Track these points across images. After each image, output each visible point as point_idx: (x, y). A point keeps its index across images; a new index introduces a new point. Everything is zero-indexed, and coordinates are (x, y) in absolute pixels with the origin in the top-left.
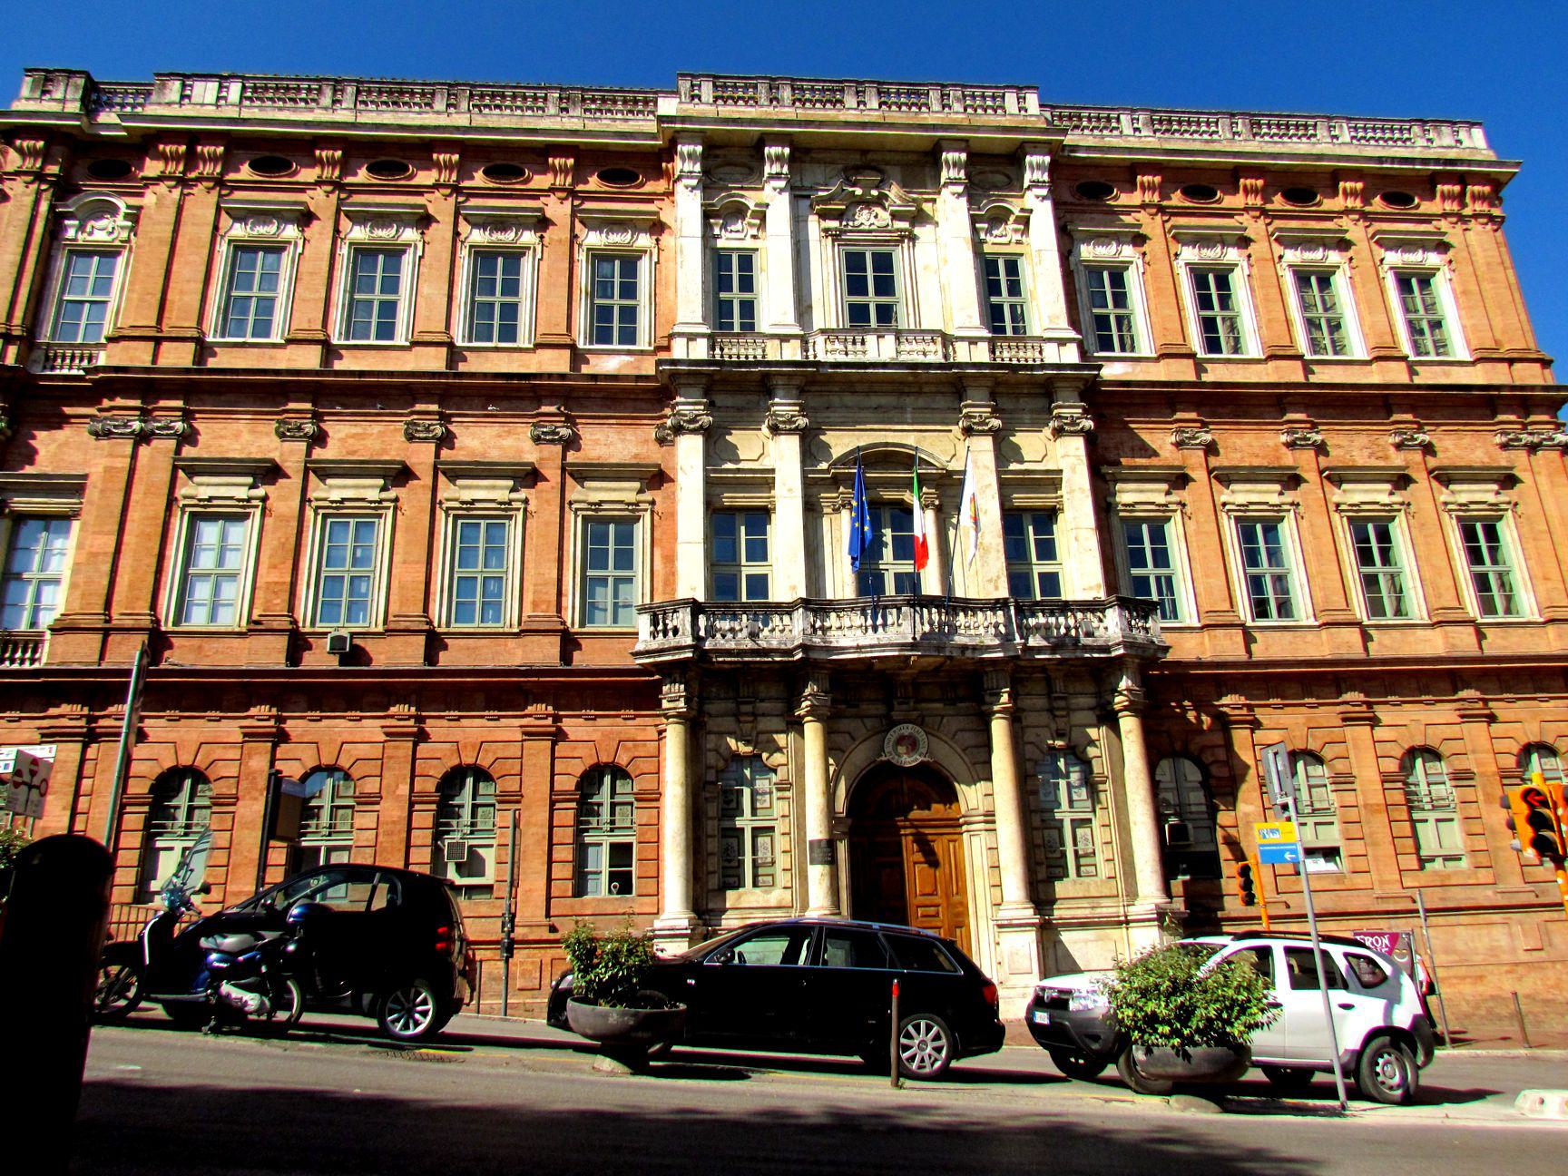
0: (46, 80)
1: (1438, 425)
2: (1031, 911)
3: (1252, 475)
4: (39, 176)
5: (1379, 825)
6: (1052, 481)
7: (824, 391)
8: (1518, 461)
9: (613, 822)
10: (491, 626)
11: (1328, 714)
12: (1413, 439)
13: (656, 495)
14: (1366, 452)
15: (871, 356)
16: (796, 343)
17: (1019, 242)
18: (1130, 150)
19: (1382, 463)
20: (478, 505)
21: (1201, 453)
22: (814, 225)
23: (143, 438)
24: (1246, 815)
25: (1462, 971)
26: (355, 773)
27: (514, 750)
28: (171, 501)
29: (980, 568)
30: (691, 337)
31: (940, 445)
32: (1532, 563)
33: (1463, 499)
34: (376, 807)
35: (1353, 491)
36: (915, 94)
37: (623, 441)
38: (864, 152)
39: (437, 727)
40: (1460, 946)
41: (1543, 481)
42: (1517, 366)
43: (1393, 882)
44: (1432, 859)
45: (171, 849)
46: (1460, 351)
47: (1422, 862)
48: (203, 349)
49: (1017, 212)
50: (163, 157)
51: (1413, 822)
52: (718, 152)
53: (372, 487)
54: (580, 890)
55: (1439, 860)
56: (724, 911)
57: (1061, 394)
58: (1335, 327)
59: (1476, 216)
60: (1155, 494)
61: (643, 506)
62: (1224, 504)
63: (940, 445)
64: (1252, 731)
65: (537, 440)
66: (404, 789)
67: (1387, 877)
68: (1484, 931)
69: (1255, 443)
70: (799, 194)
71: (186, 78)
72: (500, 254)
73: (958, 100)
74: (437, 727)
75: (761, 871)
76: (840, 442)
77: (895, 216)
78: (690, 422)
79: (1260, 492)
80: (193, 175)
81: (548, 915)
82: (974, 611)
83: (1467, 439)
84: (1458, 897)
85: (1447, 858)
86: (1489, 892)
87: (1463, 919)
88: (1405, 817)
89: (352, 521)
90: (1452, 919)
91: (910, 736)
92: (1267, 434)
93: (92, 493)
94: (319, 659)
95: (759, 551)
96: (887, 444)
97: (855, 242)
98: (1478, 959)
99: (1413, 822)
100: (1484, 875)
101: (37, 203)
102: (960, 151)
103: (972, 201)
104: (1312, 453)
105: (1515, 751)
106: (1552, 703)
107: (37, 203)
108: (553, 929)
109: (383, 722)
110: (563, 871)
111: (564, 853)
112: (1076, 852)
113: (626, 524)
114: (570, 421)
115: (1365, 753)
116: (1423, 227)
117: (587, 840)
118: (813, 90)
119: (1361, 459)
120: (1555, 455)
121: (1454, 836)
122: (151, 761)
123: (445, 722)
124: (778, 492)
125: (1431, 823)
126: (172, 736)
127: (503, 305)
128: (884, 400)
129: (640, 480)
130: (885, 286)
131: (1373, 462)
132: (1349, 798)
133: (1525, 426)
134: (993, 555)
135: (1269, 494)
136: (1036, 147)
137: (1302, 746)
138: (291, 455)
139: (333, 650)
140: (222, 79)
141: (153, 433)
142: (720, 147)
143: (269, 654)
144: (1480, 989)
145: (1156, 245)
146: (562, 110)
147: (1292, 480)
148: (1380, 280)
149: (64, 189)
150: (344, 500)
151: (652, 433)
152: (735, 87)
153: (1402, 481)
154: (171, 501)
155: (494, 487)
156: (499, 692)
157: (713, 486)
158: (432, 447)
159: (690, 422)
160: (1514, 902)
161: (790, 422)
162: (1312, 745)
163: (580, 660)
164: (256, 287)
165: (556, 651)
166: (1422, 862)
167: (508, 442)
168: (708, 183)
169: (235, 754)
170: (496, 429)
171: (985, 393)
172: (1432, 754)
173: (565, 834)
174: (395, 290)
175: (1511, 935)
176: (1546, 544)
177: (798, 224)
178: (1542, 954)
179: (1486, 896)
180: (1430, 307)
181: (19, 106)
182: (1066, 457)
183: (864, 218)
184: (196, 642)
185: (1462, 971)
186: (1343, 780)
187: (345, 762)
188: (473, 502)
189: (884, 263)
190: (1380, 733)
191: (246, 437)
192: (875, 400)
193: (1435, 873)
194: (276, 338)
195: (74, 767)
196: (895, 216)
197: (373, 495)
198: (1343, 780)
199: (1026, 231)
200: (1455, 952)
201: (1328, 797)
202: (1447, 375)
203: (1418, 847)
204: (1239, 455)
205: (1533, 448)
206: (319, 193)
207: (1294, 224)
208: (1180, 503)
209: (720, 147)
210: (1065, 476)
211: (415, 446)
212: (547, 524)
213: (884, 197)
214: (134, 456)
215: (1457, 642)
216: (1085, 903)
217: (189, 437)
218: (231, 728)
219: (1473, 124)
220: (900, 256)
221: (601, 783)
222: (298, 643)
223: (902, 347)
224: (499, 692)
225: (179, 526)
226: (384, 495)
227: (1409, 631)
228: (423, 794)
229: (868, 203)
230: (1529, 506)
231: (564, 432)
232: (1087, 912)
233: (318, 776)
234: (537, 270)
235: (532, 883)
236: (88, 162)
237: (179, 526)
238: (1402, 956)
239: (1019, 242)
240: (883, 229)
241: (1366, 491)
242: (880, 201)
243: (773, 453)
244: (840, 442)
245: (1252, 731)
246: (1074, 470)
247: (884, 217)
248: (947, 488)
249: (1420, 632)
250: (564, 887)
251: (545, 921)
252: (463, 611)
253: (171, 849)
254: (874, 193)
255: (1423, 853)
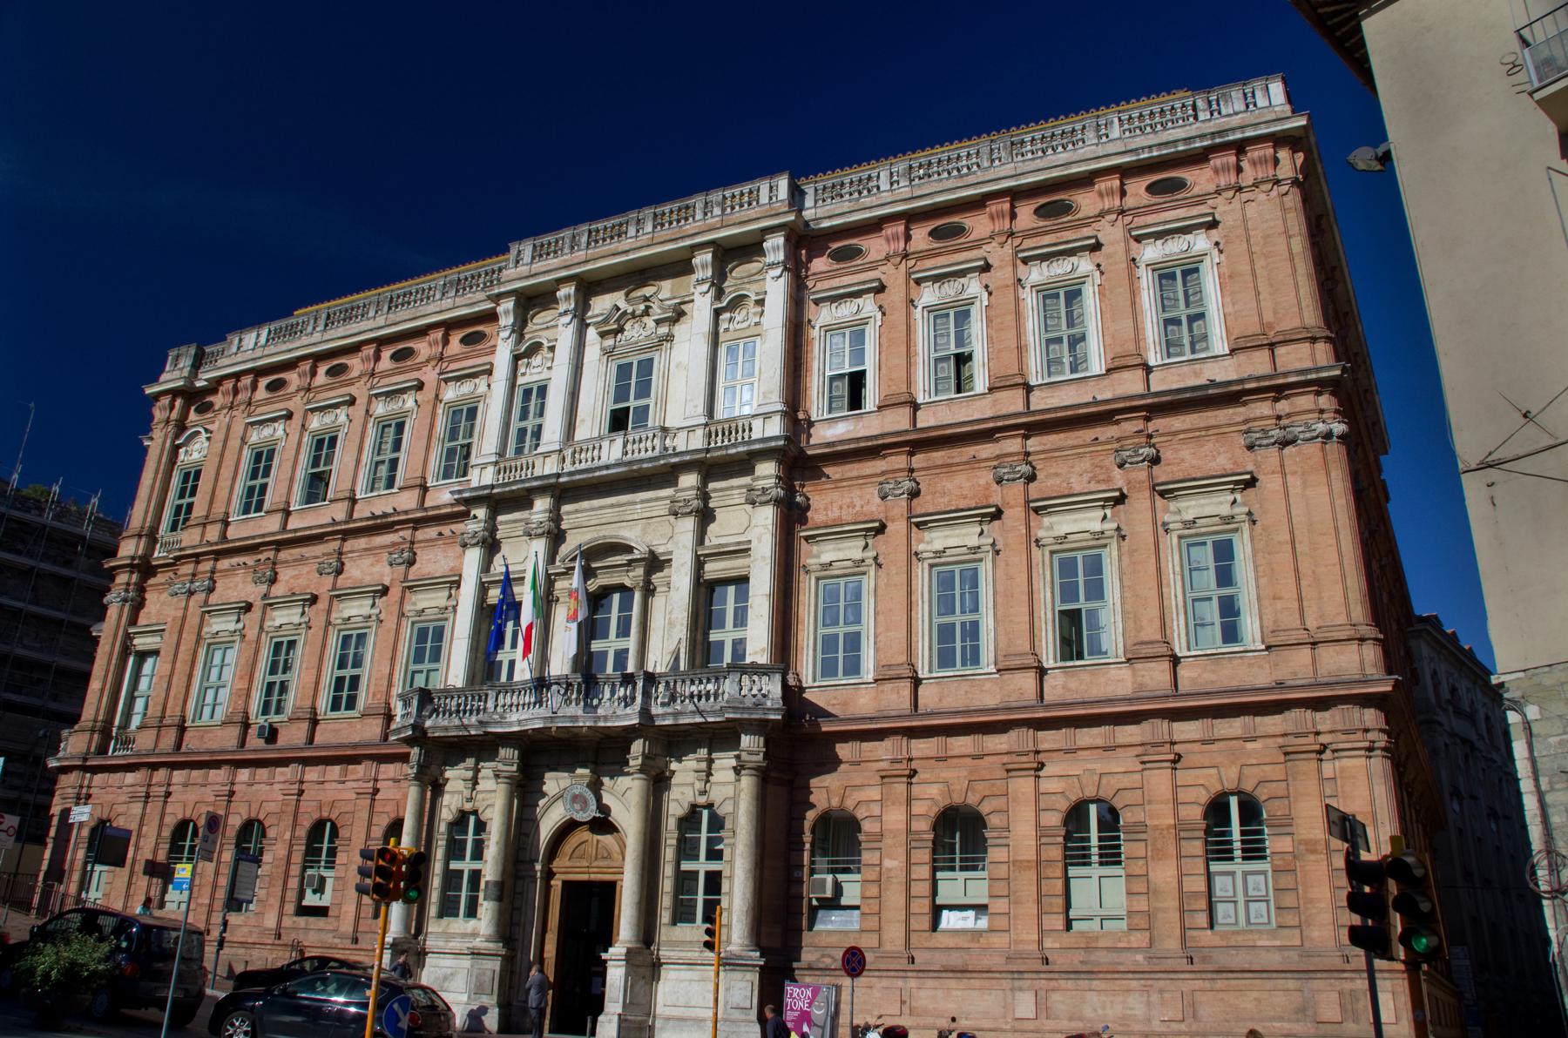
3: (950, 518)
14: (1086, 478)
17: (757, 324)
32: (1263, 581)
40: (1088, 1012)
46: (1219, 345)
49: (754, 297)
58: (1077, 340)
67: (1024, 937)
69: (967, 485)
116: (1195, 211)
148: (1133, 280)
175: (1148, 1003)
178: (1183, 1027)
210: (752, 546)
215: (1147, 680)
230: (1273, 514)
238: (819, 1008)
246: (760, 540)
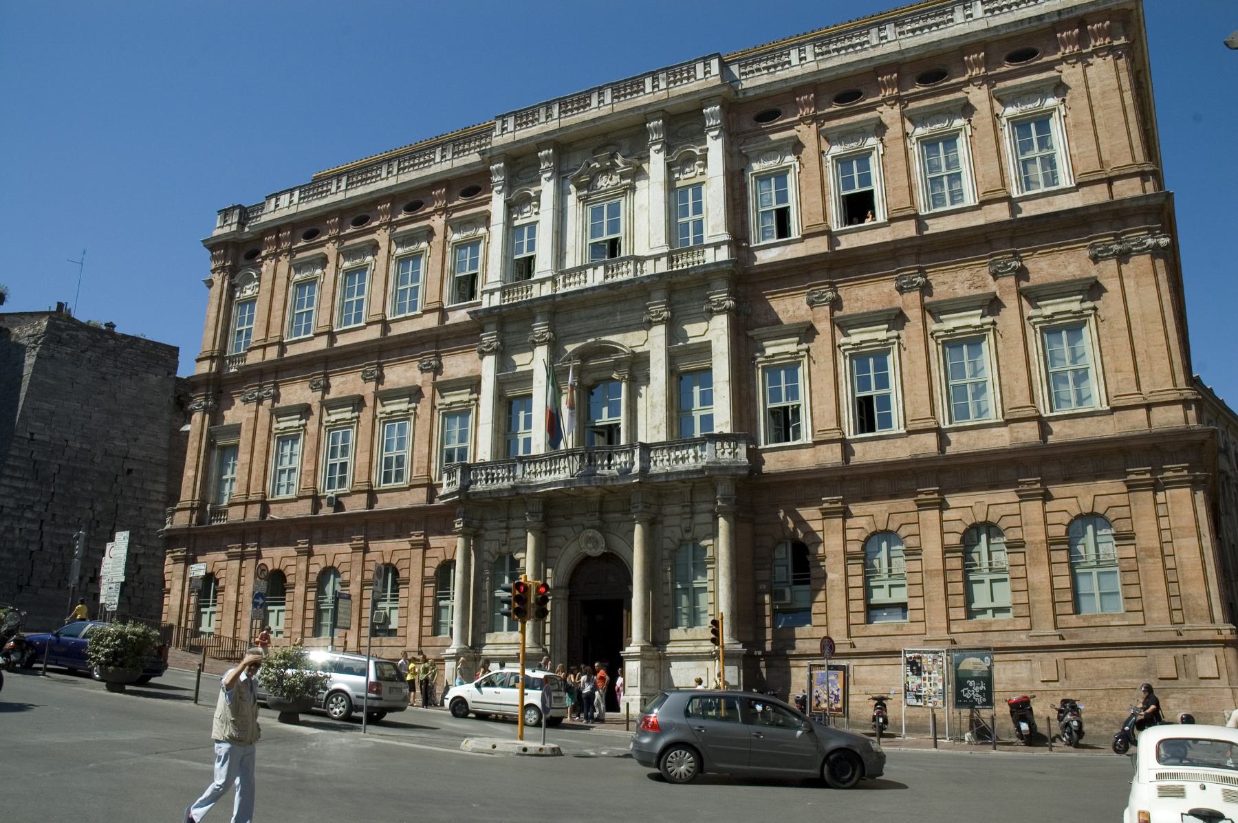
1: (1035, 251)
2: (741, 646)
5: (935, 587)
8: (1106, 272)
9: (890, 571)
10: (884, 432)
14: (967, 284)
15: (589, 284)
16: (549, 284)
17: (702, 174)
19: (980, 291)
22: (572, 200)
27: (406, 555)
28: (270, 431)
29: (652, 422)
30: (717, 246)
38: (605, 135)
43: (940, 629)
44: (983, 611)
46: (1065, 181)
48: (385, 324)
55: (990, 612)
56: (669, 641)
57: (654, 295)
60: (790, 346)
62: (1029, 318)
64: (1044, 503)
65: (422, 370)
66: (359, 578)
70: (560, 177)
77: (622, 177)
81: (420, 645)
82: (535, 463)
83: (1062, 258)
85: (996, 610)
86: (1023, 636)
92: (884, 283)
97: (596, 202)
100: (1024, 623)
102: (658, 119)
103: (668, 153)
110: (427, 622)
111: (428, 612)
113: (881, 355)
114: (922, 272)
115: (933, 531)
117: (872, 584)
119: (962, 290)
120: (1145, 259)
124: (535, 383)
128: (604, 310)
129: (980, 307)
131: (974, 292)
137: (873, 530)
139: (329, 505)
145: (894, 130)
149: (233, 271)
150: (862, 342)
154: (270, 431)
157: (500, 384)
158: (374, 383)
160: (1153, 640)
161: (542, 337)
164: (691, 224)
165: (424, 496)
168: (509, 186)
169: (294, 562)
170: (404, 367)
172: (991, 529)
173: (429, 601)
177: (561, 195)
179: (1022, 639)
180: (952, 163)
182: (715, 332)
186: (913, 553)
187: (1100, 509)
192: (599, 311)
193: (981, 622)
194: (418, 312)
195: (237, 571)
196: (622, 177)
198: (913, 553)
199: (705, 166)
202: (1050, 204)
207: (927, 102)
211: (1101, 264)
213: (615, 165)
214: (257, 411)
216: (691, 644)
217: (276, 398)
221: (979, 540)
222: (316, 500)
225: (273, 443)
228: (368, 580)
229: (606, 171)
233: (875, 538)
234: (427, 263)
235: (414, 629)
237: (273, 443)
239: (702, 174)
245: (1044, 503)
246: (718, 339)
247: (616, 179)
248: (637, 366)
250: (428, 631)
251: (1054, 632)
252: (387, 479)
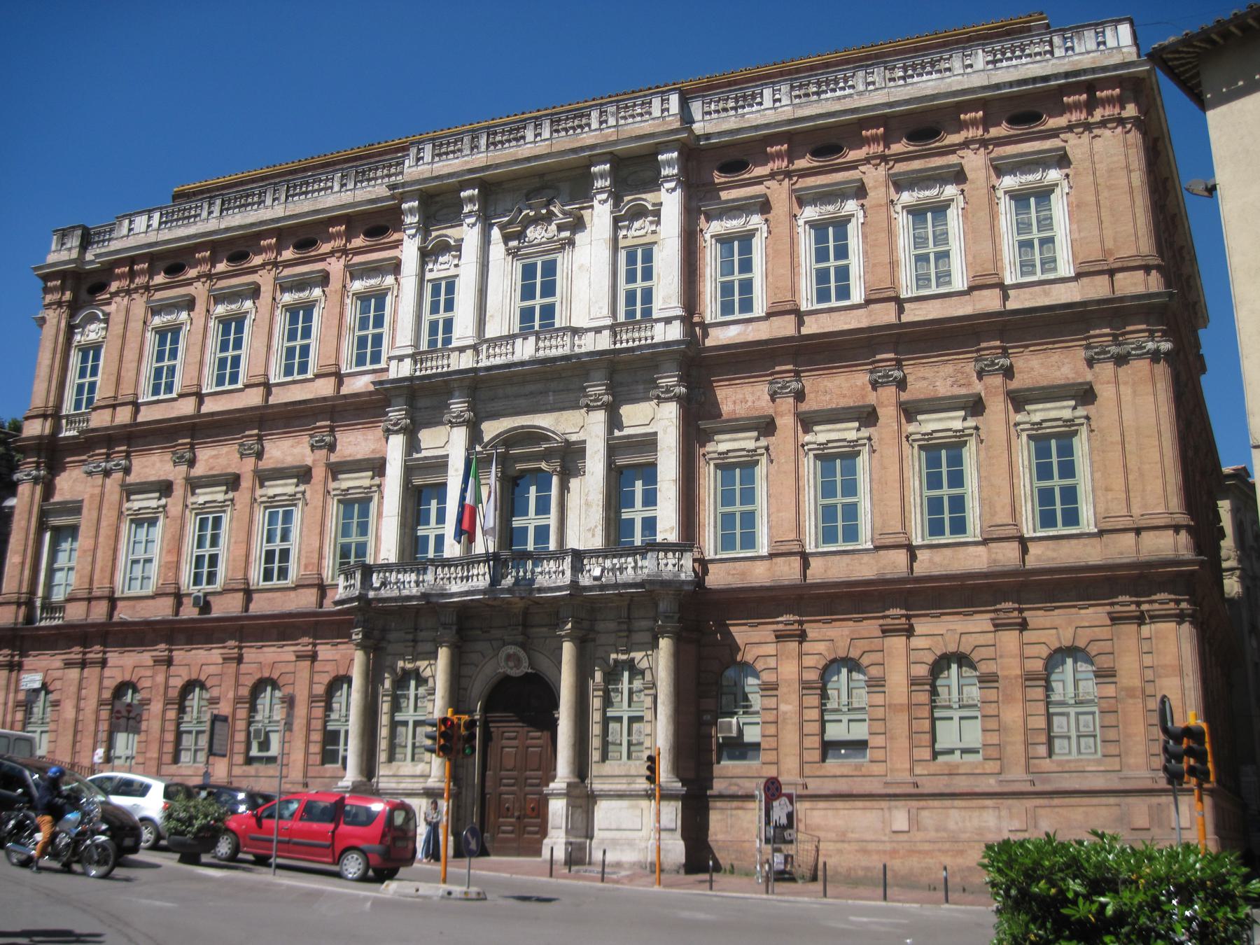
0: (64, 234)
1: (1027, 346)
4: (59, 304)
5: (899, 724)
6: (649, 443)
7: (487, 390)
11: (871, 627)
12: (993, 364)
13: (1090, 410)
15: (517, 357)
17: (654, 232)
18: (757, 128)
19: (963, 391)
20: (935, 435)
21: (791, 400)
23: (107, 473)
24: (785, 713)
25: (947, 846)
26: (208, 684)
27: (290, 668)
31: (561, 424)
33: (1037, 418)
34: (995, 685)
35: (927, 421)
36: (515, 133)
37: (366, 440)
39: (250, 654)
40: (952, 825)
41: (1126, 391)
42: (1119, 276)
45: (951, 718)
46: (1065, 268)
47: (935, 755)
50: (119, 277)
51: (933, 720)
52: (438, 199)
53: (750, 438)
54: (176, 759)
55: (958, 753)
59: (1103, 124)
61: (374, 489)
63: (561, 424)
64: (801, 643)
68: (976, 813)
71: (130, 216)
72: (233, 320)
73: (613, 114)
74: (250, 654)
75: (632, 748)
76: (491, 429)
78: (395, 425)
79: (839, 430)
80: (132, 286)
84: (962, 784)
85: (964, 751)
86: (992, 781)
87: (958, 803)
88: (1043, 711)
89: (281, 510)
90: (948, 803)
91: (515, 654)
92: (856, 375)
93: (85, 511)
94: (189, 612)
95: (650, 499)
96: (523, 427)
97: (528, 256)
98: (964, 836)
99: (933, 720)
100: (992, 766)
101: (59, 322)
104: (893, 389)
105: (1045, 655)
106: (1091, 610)
107: (59, 322)
108: (916, 785)
109: (881, 622)
110: (169, 748)
112: (629, 741)
113: (1066, 438)
115: (900, 661)
118: (503, 133)
121: (973, 734)
122: (114, 675)
123: (851, 623)
125: (956, 719)
126: (121, 663)
127: (836, 268)
129: (1072, 398)
130: (549, 289)
132: (878, 699)
133: (1115, 337)
134: (594, 509)
135: (954, 421)
136: (666, 147)
138: (177, 474)
139: (194, 605)
140: (149, 212)
141: (1129, 354)
142: (438, 195)
143: (161, 610)
144: (960, 861)
146: (1067, 49)
147: (868, 417)
149: (74, 308)
151: (1082, 353)
152: (448, 144)
153: (975, 406)
155: (286, 485)
156: (282, 628)
159: (395, 425)
162: (854, 654)
163: (254, 608)
166: (935, 755)
167: (297, 450)
169: (149, 673)
171: (401, 400)
172: (963, 659)
174: (1050, 227)
175: (999, 817)
176: (1116, 454)
181: (52, 258)
182: (658, 419)
183: (534, 233)
184: (131, 603)
185: (947, 846)
186: (876, 684)
188: (275, 496)
189: (550, 269)
190: (915, 642)
191: (158, 465)
197: (220, 497)
198: (876, 684)
199: (658, 223)
200: (945, 830)
201: (862, 697)
202: (1046, 294)
203: (934, 740)
204: (828, 397)
205: (1121, 360)
206: (198, 285)
208: (1088, 418)
209: (438, 195)
212: (315, 508)
214: (103, 486)
215: (1000, 557)
216: (624, 780)
218: (146, 657)
219: (1120, 21)
220: (562, 260)
223: (541, 344)
224: (282, 628)
226: (861, 434)
227: (961, 549)
229: (535, 221)
231: (897, 373)
232: (624, 787)
236: (84, 288)
240: (550, 240)
241: (940, 420)
242: (549, 217)
243: (448, 443)
244: (491, 429)
246: (665, 432)
249: (971, 549)
250: (167, 758)
253: (951, 718)
254: (544, 211)
255: (938, 746)
